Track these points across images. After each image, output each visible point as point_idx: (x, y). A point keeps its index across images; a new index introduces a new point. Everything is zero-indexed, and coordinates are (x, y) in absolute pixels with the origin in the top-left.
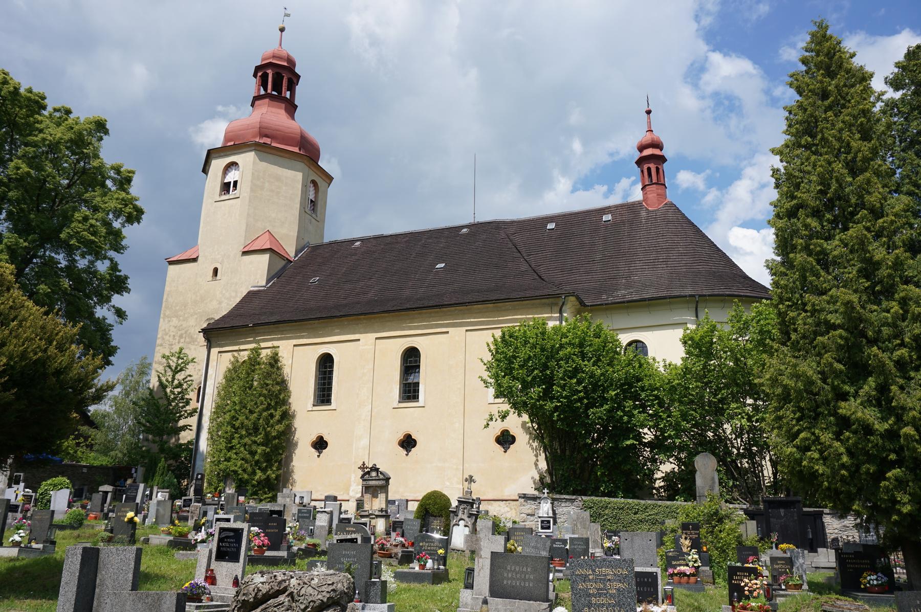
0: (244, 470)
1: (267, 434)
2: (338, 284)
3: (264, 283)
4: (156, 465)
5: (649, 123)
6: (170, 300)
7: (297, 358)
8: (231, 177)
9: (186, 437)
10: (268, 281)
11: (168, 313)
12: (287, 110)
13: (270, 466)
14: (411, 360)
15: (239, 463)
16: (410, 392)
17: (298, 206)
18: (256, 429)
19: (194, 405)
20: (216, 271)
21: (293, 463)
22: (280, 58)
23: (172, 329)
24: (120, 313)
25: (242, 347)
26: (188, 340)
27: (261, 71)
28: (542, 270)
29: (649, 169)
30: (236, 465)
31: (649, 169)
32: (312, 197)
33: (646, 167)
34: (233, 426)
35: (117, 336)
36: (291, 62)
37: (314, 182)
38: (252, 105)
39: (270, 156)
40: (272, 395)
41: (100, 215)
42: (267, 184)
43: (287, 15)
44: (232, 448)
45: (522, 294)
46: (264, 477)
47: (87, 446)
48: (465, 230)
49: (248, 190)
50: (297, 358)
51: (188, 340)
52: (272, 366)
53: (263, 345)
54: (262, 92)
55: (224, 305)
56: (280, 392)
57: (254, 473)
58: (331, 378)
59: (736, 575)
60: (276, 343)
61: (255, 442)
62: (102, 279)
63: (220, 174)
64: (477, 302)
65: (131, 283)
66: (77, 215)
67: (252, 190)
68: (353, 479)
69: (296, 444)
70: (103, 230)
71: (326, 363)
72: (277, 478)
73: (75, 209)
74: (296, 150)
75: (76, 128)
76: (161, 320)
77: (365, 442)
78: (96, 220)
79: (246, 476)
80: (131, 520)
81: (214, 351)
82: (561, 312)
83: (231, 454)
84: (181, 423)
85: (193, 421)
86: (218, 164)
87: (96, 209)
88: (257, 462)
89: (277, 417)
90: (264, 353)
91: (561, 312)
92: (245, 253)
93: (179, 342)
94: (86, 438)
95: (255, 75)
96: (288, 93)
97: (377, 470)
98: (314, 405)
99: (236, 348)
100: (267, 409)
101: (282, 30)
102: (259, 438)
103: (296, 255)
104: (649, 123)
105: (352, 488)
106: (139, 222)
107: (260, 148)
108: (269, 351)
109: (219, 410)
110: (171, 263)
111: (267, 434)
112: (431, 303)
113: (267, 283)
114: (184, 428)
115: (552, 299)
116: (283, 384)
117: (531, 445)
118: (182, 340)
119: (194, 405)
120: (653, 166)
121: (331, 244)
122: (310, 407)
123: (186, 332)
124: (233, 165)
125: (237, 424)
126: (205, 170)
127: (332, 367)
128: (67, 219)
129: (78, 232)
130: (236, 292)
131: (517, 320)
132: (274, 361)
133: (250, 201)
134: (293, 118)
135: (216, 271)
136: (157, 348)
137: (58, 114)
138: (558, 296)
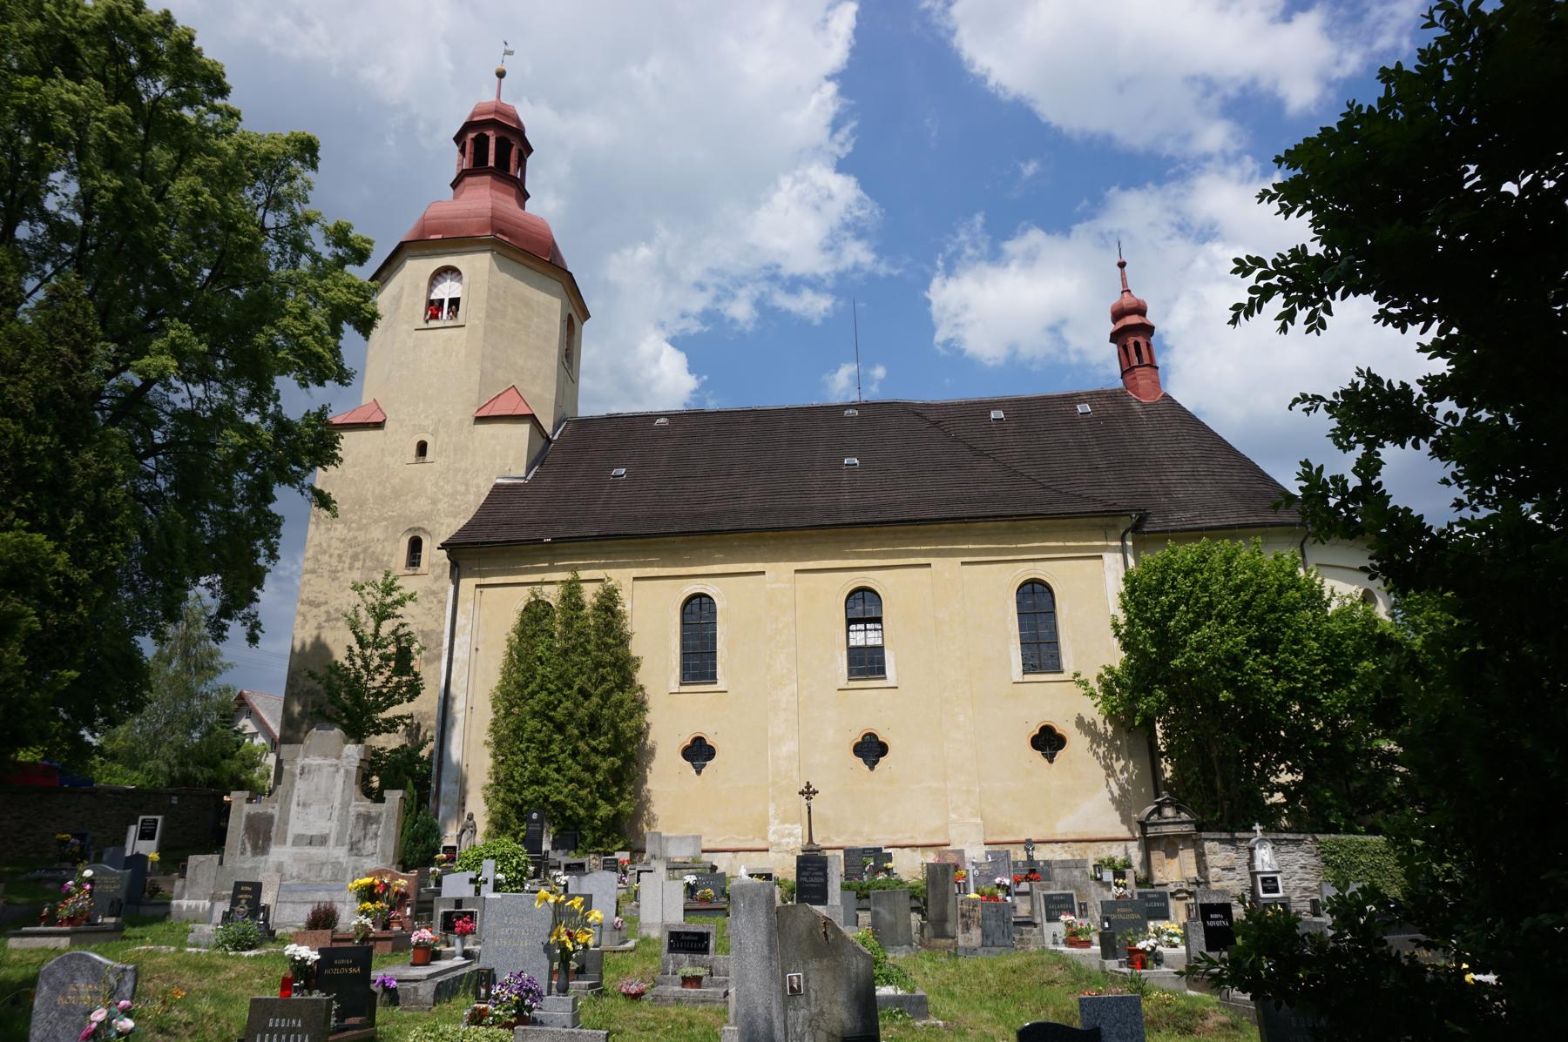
3: (522, 473)
5: (1124, 279)
7: (649, 602)
14: (863, 607)
17: (556, 351)
20: (422, 449)
21: (649, 786)
23: (335, 543)
26: (369, 564)
29: (1137, 344)
31: (1137, 344)
33: (1131, 341)
39: (513, 264)
42: (510, 310)
43: (510, 53)
44: (548, 760)
49: (482, 315)
50: (649, 602)
51: (369, 564)
53: (583, 575)
57: (594, 806)
60: (611, 573)
61: (594, 750)
63: (425, 284)
64: (985, 518)
67: (488, 316)
68: (772, 812)
69: (652, 752)
71: (698, 616)
76: (312, 527)
83: (548, 770)
90: (589, 594)
92: (480, 420)
93: (351, 568)
98: (1025, 672)
101: (501, 74)
102: (603, 743)
104: (1124, 279)
105: (772, 828)
113: (528, 473)
117: (1095, 753)
118: (358, 564)
120: (1141, 340)
123: (365, 551)
125: (559, 714)
127: (1051, 612)
130: (467, 485)
132: (608, 603)
133: (485, 334)
134: (523, 207)
135: (422, 449)
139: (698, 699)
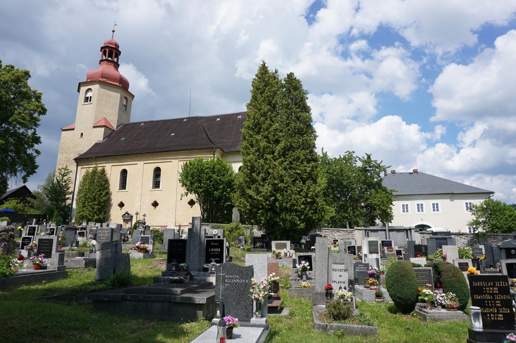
0: (90, 215)
1: (99, 201)
2: (134, 140)
3: (102, 140)
4: (53, 213)
6: (63, 146)
7: (112, 171)
8: (89, 95)
9: (69, 202)
10: (104, 139)
11: (61, 151)
12: (114, 66)
13: (100, 213)
14: (157, 172)
15: (88, 212)
16: (157, 184)
17: (118, 108)
18: (95, 199)
19: (70, 190)
20: (82, 134)
22: (112, 44)
23: (64, 158)
24: (38, 152)
25: (90, 166)
27: (104, 49)
28: (212, 138)
30: (86, 213)
32: (125, 104)
34: (86, 198)
35: (38, 160)
36: (117, 46)
37: (126, 98)
38: (100, 63)
40: (101, 185)
41: (27, 111)
43: (116, 25)
44: (85, 206)
45: (200, 147)
46: (98, 218)
47: (29, 206)
48: (185, 120)
50: (112, 171)
52: (102, 174)
53: (99, 165)
54: (104, 58)
55: (85, 148)
56: (105, 184)
57: (94, 216)
58: (126, 179)
59: (358, 266)
60: (104, 165)
61: (94, 204)
62: (29, 138)
63: (84, 93)
65: (42, 140)
66: (16, 112)
67: (97, 101)
69: (112, 205)
70: (28, 118)
71: (124, 173)
72: (104, 218)
73: (15, 109)
74: (118, 84)
75: (16, 74)
77: (139, 204)
78: (25, 114)
79: (90, 218)
80: (20, 229)
81: (79, 168)
82: (214, 155)
84: (67, 196)
85: (71, 196)
86: (83, 89)
87: (25, 109)
88: (95, 212)
89: (104, 194)
90: (99, 169)
91: (214, 155)
92: (94, 127)
94: (29, 202)
95: (101, 51)
96: (116, 59)
97: (128, 214)
99: (88, 166)
100: (100, 191)
101: (113, 31)
102: (96, 203)
103: (117, 128)
106: (45, 114)
107: (101, 83)
108: (101, 168)
109: (80, 191)
110: (63, 130)
111: (99, 201)
112: (166, 150)
114: (68, 199)
115: (211, 149)
116: (107, 181)
119: (70, 190)
121: (132, 124)
122: (118, 190)
124: (89, 90)
126: (79, 91)
128: (12, 113)
129: (16, 119)
131: (193, 158)
132: (103, 171)
135: (82, 134)
136: (57, 166)
137: (8, 68)
138: (213, 148)
139: (123, 192)
